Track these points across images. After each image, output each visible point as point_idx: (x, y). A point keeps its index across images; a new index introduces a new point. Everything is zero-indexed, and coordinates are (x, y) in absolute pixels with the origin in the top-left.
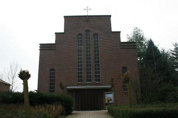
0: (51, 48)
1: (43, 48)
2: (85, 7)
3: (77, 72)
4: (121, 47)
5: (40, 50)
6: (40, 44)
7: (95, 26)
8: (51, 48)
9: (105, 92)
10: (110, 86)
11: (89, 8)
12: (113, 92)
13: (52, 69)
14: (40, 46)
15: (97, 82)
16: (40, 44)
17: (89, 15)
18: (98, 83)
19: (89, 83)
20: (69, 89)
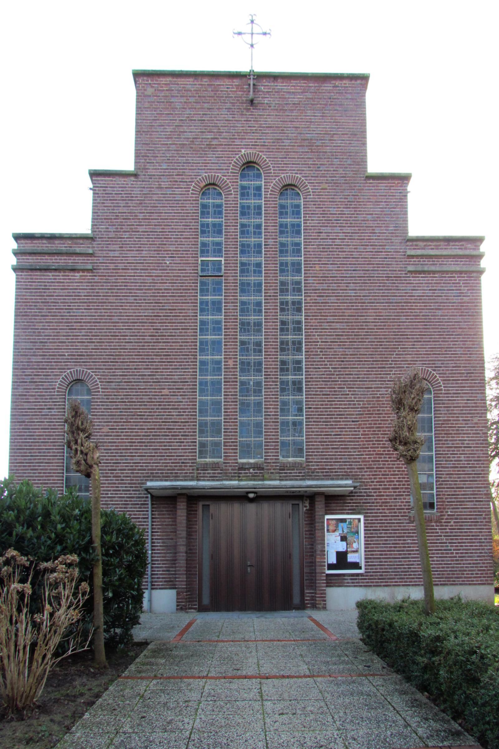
0: (70, 261)
1: (32, 260)
2: (262, 25)
3: (200, 262)
4: (410, 268)
5: (15, 269)
6: (18, 237)
7: (287, 142)
8: (70, 261)
9: (327, 514)
10: (349, 482)
11: (262, 25)
12: (361, 517)
13: (78, 381)
14: (14, 245)
15: (290, 459)
16: (18, 237)
17: (261, 67)
18: (294, 466)
19: (252, 461)
20: (155, 493)
